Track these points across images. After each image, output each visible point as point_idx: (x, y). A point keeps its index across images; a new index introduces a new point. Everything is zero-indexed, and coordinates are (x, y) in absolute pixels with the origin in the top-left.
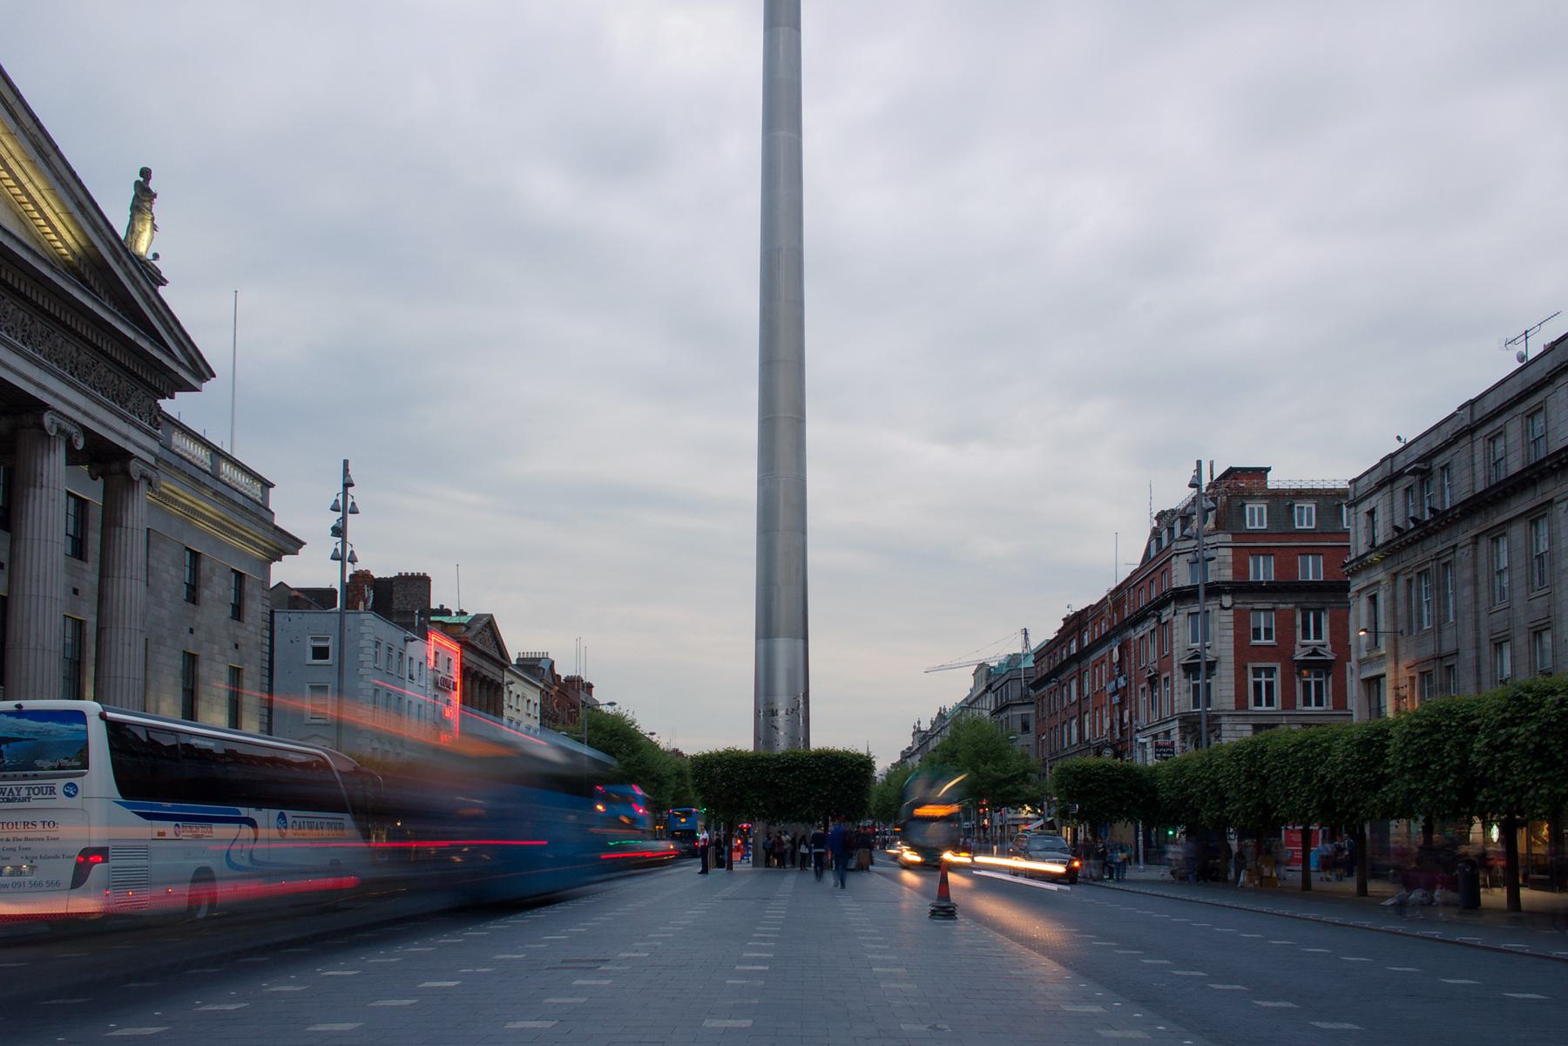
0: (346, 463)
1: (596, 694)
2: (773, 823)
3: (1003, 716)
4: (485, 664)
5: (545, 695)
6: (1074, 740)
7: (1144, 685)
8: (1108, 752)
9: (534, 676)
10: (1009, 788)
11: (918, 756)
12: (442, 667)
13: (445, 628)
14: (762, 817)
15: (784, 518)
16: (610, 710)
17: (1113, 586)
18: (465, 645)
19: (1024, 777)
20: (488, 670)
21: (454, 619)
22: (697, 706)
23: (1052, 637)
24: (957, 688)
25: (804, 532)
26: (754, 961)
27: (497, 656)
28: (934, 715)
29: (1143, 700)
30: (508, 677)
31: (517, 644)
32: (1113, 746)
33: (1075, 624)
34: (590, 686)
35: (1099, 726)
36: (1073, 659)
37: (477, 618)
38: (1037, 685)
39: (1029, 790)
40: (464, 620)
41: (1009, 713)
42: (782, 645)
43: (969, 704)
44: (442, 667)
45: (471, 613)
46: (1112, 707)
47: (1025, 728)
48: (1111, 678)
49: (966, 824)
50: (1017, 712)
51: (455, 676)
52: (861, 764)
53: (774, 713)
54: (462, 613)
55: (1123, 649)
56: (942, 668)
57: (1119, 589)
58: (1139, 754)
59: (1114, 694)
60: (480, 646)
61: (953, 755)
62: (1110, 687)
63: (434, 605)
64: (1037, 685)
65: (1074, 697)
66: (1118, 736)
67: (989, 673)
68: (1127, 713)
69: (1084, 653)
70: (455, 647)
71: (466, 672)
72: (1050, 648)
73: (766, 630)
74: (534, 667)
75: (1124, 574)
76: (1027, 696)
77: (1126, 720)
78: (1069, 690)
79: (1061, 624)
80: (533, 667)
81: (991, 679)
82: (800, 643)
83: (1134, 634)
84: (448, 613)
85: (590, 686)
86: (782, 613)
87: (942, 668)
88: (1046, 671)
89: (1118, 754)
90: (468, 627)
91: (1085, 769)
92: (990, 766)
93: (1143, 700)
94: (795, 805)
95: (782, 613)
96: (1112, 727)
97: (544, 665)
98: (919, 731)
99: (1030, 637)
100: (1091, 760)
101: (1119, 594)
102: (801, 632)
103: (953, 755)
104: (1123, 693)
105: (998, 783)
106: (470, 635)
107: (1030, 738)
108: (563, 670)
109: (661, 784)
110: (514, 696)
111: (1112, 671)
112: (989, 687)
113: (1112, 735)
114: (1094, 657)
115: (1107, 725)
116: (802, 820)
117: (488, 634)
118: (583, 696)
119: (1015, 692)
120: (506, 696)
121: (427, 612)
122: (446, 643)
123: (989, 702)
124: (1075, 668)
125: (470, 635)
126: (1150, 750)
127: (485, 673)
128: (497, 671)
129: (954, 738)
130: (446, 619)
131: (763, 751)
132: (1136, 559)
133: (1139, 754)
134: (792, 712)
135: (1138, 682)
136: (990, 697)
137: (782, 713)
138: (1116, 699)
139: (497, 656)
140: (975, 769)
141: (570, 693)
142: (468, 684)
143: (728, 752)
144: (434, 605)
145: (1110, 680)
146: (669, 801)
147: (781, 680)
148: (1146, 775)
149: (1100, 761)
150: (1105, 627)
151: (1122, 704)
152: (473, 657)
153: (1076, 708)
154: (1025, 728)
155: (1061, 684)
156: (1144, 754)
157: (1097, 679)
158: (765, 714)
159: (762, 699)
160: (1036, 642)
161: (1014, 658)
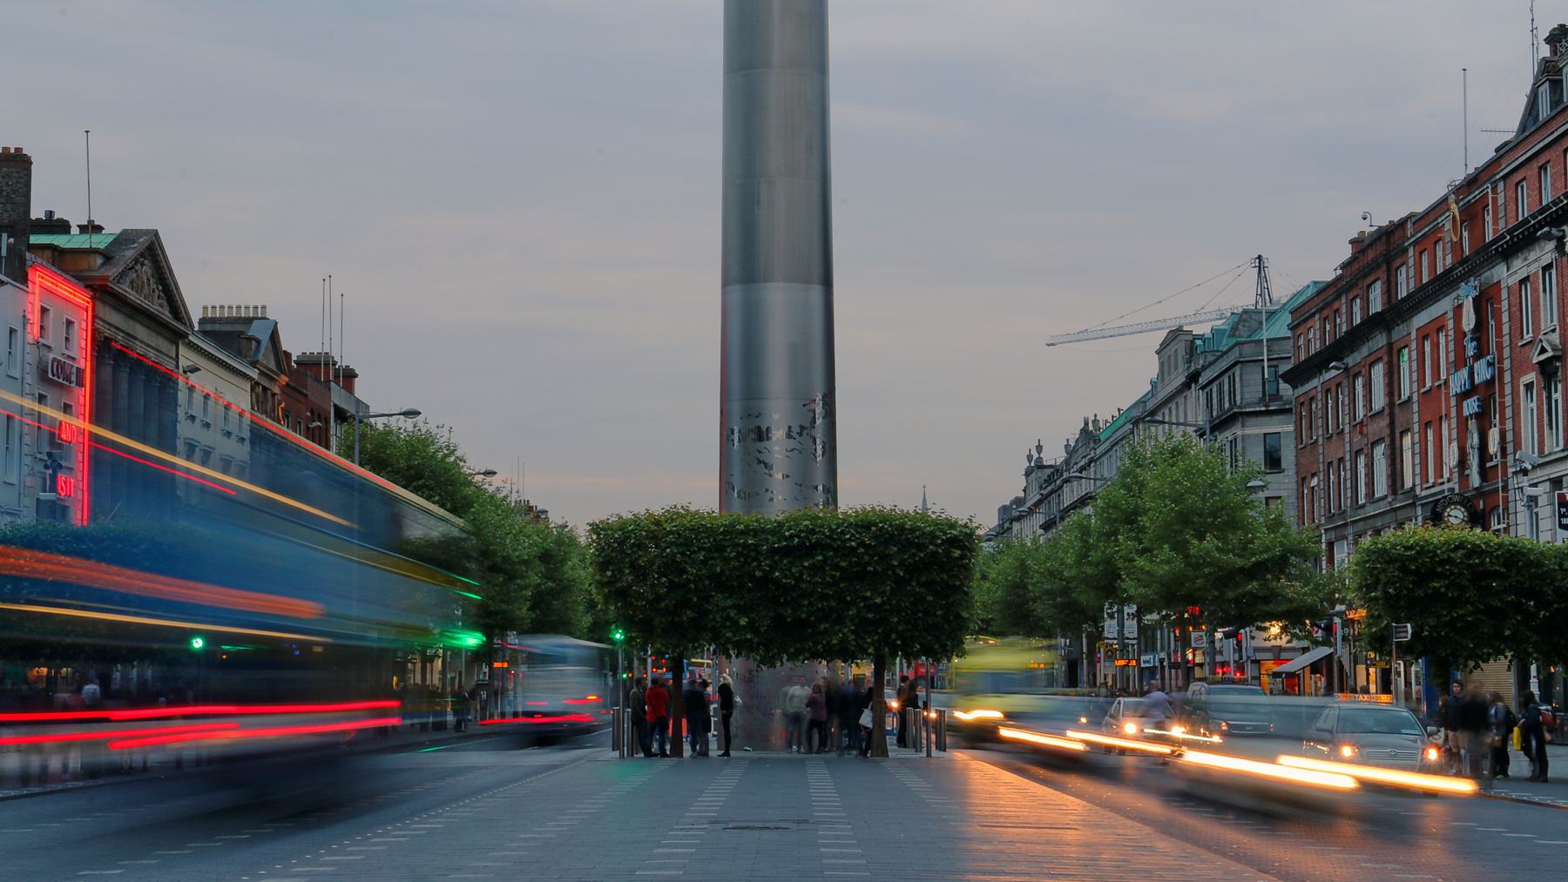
0: (1259, 257)
1: (361, 389)
2: (769, 661)
3: (1225, 436)
4: (140, 331)
5: (255, 385)
6: (1381, 488)
7: (1531, 377)
8: (1456, 515)
9: (239, 354)
10: (1253, 586)
11: (1039, 519)
12: (54, 337)
13: (61, 258)
14: (744, 648)
15: (781, 39)
16: (407, 424)
17: (1459, 177)
18: (102, 292)
19: (1279, 564)
20: (146, 343)
21: (74, 240)
22: (590, 411)
23: (1329, 275)
24: (1126, 376)
25: (822, 69)
26: (378, 844)
27: (166, 315)
28: (1073, 433)
29: (1529, 407)
30: (187, 357)
31: (203, 290)
32: (1465, 502)
33: (1379, 251)
34: (349, 376)
35: (1436, 459)
36: (1374, 323)
37: (125, 238)
38: (1297, 376)
39: (1291, 589)
40: (99, 241)
41: (1237, 430)
42: (781, 301)
43: (1146, 414)
44: (54, 337)
45: (112, 228)
46: (1463, 423)
47: (1273, 461)
48: (1460, 362)
49: (1148, 660)
50: (1256, 429)
51: (80, 353)
52: (953, 542)
53: (761, 435)
54: (91, 228)
55: (1485, 301)
56: (1084, 336)
57: (1472, 182)
58: (1523, 517)
59: (1464, 396)
60: (133, 296)
61: (1131, 518)
62: (1458, 381)
63: (37, 213)
64: (1297, 376)
65: (1379, 401)
66: (1475, 480)
67: (1192, 350)
68: (1494, 436)
69: (1398, 312)
70: (82, 298)
71: (102, 347)
72: (1326, 298)
73: (745, 265)
74: (235, 337)
75: (1483, 154)
76: (1276, 396)
77: (1493, 447)
78: (1368, 386)
79: (1347, 253)
80: (239, 335)
81: (1193, 361)
82: (816, 292)
83: (1505, 275)
84: (63, 227)
85: (349, 376)
86: (777, 232)
87: (1084, 336)
88: (1315, 347)
89: (1478, 518)
90: (107, 256)
91: (1423, 550)
92: (1210, 542)
93: (1529, 407)
94: (787, 614)
95: (777, 232)
96: (1463, 463)
97: (259, 331)
98: (1041, 467)
99: (1271, 273)
100: (1416, 531)
101: (1471, 194)
102: (817, 271)
103: (1131, 518)
104: (1486, 392)
105: (1228, 577)
106: (112, 272)
107: (1283, 484)
108: (296, 344)
109: (511, 577)
110: (198, 397)
111: (1460, 348)
112: (1193, 378)
113: (1464, 478)
114: (1422, 319)
115: (1451, 456)
116: (830, 654)
117: (146, 269)
118: (337, 396)
119: (1249, 389)
120: (182, 396)
121: (22, 226)
122: (64, 290)
123: (1195, 409)
124: (1380, 340)
125: (112, 272)
126: (1546, 511)
127: (140, 349)
128: (164, 345)
129: (1131, 481)
130: (60, 241)
131: (739, 512)
132: (1508, 122)
133: (1523, 517)
134: (801, 432)
135: (1517, 370)
136: (1195, 397)
137: (778, 434)
138: (1471, 406)
139: (166, 315)
140: (1180, 547)
141: (312, 391)
142: (107, 372)
143: (672, 516)
144: (37, 213)
145: (1460, 362)
146: (523, 611)
147: (776, 384)
148: (1551, 564)
149: (1436, 536)
150: (1444, 261)
151: (1483, 418)
152: (115, 318)
153: (1384, 423)
154: (1273, 461)
155: (1351, 374)
156: (1535, 520)
157: (1427, 362)
158: (743, 433)
159: (736, 407)
160: (1289, 283)
161: (1245, 320)
